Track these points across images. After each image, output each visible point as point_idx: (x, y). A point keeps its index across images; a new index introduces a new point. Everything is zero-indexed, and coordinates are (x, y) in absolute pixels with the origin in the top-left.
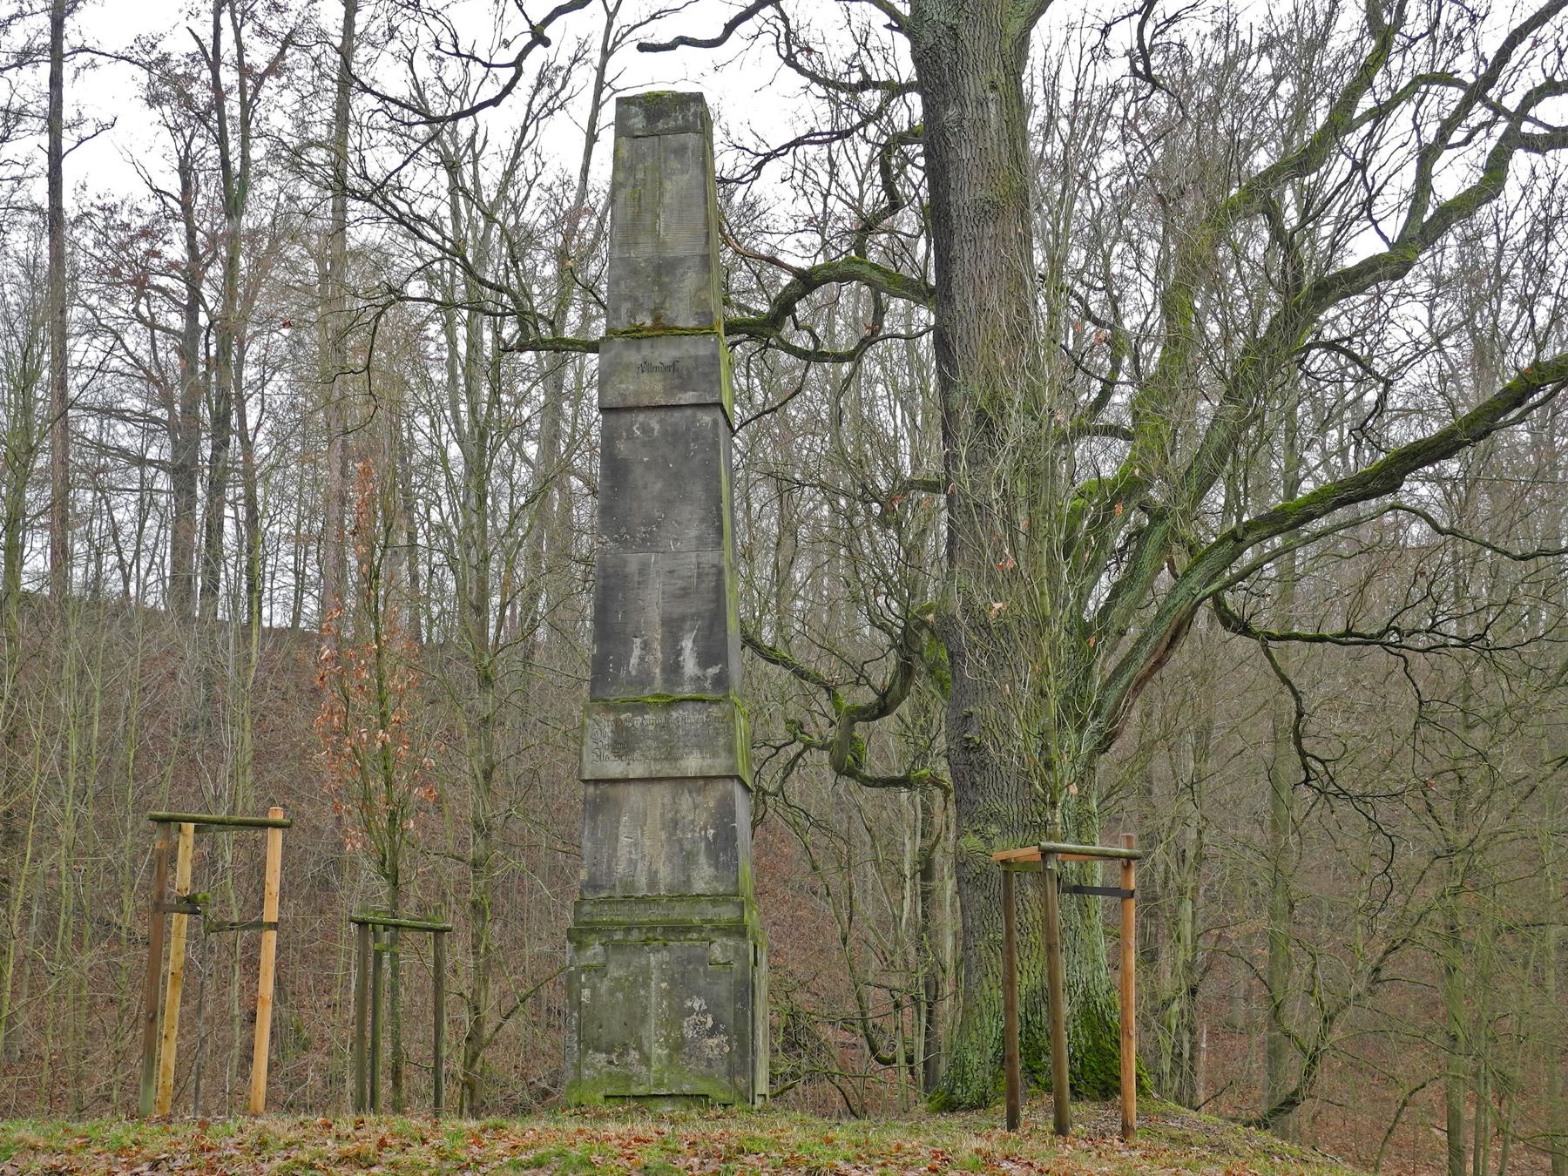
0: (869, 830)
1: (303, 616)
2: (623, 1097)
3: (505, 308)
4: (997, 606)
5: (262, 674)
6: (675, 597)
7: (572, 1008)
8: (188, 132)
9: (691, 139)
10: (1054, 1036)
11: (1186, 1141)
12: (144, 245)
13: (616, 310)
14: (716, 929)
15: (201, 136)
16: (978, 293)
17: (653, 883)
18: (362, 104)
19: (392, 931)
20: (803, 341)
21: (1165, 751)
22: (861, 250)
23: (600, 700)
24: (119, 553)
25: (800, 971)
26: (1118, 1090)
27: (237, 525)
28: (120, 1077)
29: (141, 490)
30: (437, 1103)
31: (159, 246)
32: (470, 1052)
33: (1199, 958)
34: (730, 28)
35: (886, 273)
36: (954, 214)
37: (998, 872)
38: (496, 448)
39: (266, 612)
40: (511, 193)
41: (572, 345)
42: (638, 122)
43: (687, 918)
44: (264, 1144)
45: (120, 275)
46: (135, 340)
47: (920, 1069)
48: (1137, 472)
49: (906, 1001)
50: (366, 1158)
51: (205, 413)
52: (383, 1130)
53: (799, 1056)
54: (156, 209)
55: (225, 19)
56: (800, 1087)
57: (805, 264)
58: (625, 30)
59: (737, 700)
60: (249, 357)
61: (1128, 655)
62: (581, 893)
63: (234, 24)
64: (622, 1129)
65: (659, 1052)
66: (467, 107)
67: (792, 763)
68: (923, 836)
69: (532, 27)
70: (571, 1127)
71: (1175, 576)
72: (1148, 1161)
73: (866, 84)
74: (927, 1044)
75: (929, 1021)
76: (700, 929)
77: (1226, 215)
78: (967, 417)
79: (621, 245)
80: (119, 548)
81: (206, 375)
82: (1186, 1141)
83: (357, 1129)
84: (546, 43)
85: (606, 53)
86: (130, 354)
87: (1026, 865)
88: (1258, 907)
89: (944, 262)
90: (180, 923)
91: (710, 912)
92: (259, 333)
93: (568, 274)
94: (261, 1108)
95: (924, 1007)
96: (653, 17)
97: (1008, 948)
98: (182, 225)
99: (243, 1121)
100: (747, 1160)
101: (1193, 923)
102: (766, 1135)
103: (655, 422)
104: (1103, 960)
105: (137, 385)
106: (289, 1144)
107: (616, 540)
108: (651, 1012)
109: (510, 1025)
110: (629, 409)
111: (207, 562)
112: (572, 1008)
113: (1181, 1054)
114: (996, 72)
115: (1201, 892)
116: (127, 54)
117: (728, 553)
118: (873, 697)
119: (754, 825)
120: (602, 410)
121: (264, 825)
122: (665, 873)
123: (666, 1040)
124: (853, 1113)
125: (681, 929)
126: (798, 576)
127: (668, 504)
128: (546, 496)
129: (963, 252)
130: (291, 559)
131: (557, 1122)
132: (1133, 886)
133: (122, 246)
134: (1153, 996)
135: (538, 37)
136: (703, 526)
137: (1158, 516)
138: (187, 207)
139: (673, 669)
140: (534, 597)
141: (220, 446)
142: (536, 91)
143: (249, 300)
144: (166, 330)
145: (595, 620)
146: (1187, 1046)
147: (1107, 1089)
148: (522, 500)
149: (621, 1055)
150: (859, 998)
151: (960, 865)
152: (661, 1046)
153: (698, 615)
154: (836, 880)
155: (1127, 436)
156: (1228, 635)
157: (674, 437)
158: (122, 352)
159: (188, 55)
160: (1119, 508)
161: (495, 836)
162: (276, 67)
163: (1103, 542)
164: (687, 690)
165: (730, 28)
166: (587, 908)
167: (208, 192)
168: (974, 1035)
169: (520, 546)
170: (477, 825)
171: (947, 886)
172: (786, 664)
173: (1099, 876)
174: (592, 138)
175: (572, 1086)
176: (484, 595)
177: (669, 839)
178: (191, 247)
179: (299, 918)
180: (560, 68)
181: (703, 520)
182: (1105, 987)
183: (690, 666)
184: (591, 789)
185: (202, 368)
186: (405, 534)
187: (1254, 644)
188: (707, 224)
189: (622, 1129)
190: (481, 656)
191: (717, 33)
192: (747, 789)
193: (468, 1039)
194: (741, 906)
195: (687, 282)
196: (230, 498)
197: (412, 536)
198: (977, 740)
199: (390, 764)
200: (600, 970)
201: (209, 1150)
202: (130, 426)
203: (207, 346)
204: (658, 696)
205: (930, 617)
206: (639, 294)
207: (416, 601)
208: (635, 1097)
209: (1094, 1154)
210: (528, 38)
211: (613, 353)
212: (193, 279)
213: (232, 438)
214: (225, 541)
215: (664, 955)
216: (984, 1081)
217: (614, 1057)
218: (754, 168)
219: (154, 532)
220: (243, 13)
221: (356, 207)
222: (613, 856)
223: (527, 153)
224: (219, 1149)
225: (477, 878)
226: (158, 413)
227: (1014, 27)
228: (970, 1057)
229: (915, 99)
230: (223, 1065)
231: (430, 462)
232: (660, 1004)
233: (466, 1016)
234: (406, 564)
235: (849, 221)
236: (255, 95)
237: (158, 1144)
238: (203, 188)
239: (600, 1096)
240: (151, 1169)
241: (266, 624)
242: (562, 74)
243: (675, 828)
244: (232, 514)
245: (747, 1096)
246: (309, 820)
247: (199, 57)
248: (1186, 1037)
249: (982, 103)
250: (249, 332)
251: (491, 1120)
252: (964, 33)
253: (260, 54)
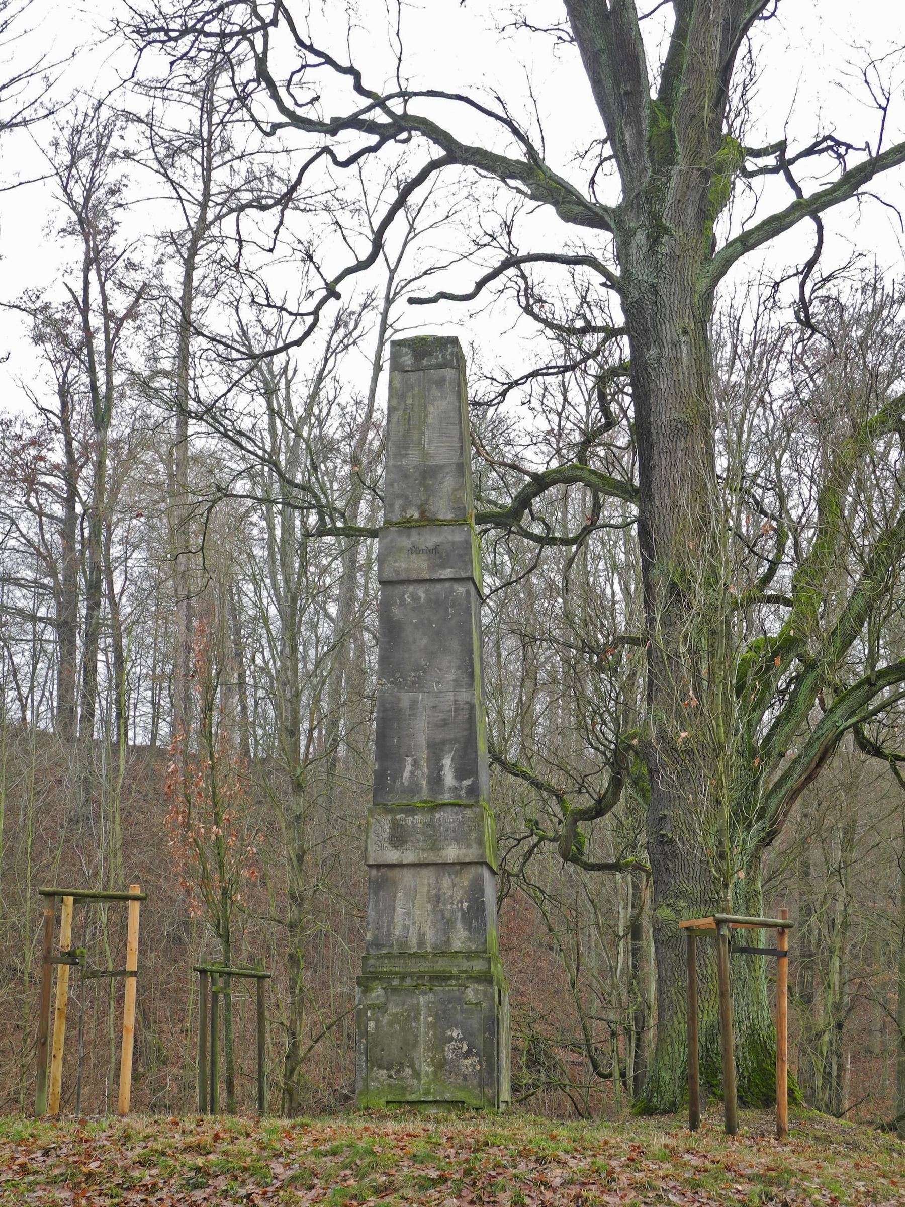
0: (592, 902)
1: (159, 737)
2: (400, 1102)
3: (310, 503)
4: (684, 734)
5: (128, 781)
6: (437, 726)
7: (361, 1036)
8: (65, 364)
9: (449, 373)
10: (726, 1059)
11: (827, 1140)
12: (33, 452)
13: (392, 506)
14: (469, 977)
15: (75, 367)
16: (672, 493)
17: (421, 943)
18: (197, 344)
19: (225, 977)
20: (537, 529)
21: (819, 844)
22: (582, 458)
23: (380, 804)
24: (18, 688)
25: (540, 1007)
26: (775, 1100)
27: (108, 667)
28: (25, 1084)
29: (33, 640)
30: (261, 1107)
31: (44, 453)
32: (289, 1067)
33: (846, 999)
34: (480, 285)
35: (601, 476)
36: (654, 432)
37: (685, 934)
38: (303, 610)
39: (130, 734)
40: (316, 411)
41: (361, 532)
42: (408, 360)
43: (448, 969)
44: (128, 1137)
45: (15, 475)
46: (27, 524)
47: (630, 1082)
48: (792, 633)
49: (620, 1031)
50: (205, 1147)
51: (81, 581)
52: (218, 1127)
53: (539, 1071)
54: (41, 423)
55: (93, 276)
56: (540, 1093)
57: (542, 469)
58: (403, 283)
59: (485, 804)
60: (115, 538)
61: (786, 772)
62: (367, 950)
63: (100, 279)
64: (397, 1127)
65: (426, 1069)
66: (280, 344)
67: (530, 852)
68: (633, 906)
69: (326, 284)
70: (360, 1125)
71: (824, 711)
72: (797, 1155)
73: (589, 328)
74: (636, 1063)
75: (638, 1046)
76: (457, 977)
77: (866, 433)
78: (661, 589)
79: (395, 455)
80: (17, 684)
81: (82, 552)
82: (827, 1140)
83: (198, 1126)
84: (338, 296)
85: (389, 301)
86: (23, 536)
87: (705, 932)
88: (889, 964)
89: (646, 470)
90: (63, 971)
91: (465, 964)
92: (123, 519)
93: (357, 478)
94: (127, 1110)
95: (634, 1036)
96: (425, 273)
97: (692, 992)
98: (61, 436)
99: (113, 1119)
100: (491, 1151)
101: (840, 973)
102: (506, 1132)
103: (421, 592)
104: (765, 1002)
105: (29, 560)
106: (147, 1137)
107: (392, 683)
108: (421, 1039)
109: (319, 1047)
110: (402, 582)
111: (84, 696)
112: (361, 1036)
113: (830, 1074)
114: (687, 321)
115: (847, 951)
116: (17, 303)
117: (478, 692)
118: (592, 803)
119: (500, 900)
120: (380, 583)
121: (126, 898)
122: (431, 936)
123: (432, 1061)
124: (580, 1114)
125: (443, 977)
126: (538, 707)
127: (432, 655)
128: (343, 646)
129: (661, 461)
130: (150, 693)
131: (349, 1121)
132: (786, 948)
133: (16, 452)
134: (809, 1029)
135: (332, 292)
136: (459, 672)
137: (811, 666)
138: (65, 422)
139: (436, 781)
140: (334, 723)
141: (94, 606)
142: (335, 330)
143: (114, 493)
144: (51, 517)
145: (377, 743)
146: (835, 1067)
147: (768, 1101)
148: (326, 648)
149: (398, 1071)
150: (584, 1028)
151: (657, 931)
152: (428, 1065)
153: (455, 740)
154: (567, 940)
155: (787, 603)
156: (863, 756)
157: (436, 603)
158: (17, 534)
159: (64, 304)
160: (778, 661)
161: (307, 905)
162: (132, 313)
163: (767, 685)
164: (447, 797)
165: (480, 285)
166: (372, 961)
167: (82, 410)
168: (666, 1058)
169: (324, 683)
170: (293, 897)
171: (650, 947)
172: (525, 776)
173: (763, 939)
174: (378, 368)
175: (361, 1094)
176: (296, 722)
177: (434, 909)
178: (69, 453)
179: (159, 966)
180: (353, 313)
181: (459, 668)
182: (766, 1023)
183: (449, 779)
184: (374, 872)
185: (78, 547)
186: (236, 675)
187: (887, 764)
188: (461, 439)
189: (397, 1127)
190: (295, 769)
191: (470, 289)
192: (493, 873)
193: (287, 1057)
194: (489, 960)
195: (446, 485)
196: (102, 646)
197: (242, 676)
198: (670, 835)
199: (222, 851)
200: (382, 1008)
201: (87, 1141)
202: (25, 591)
203: (82, 529)
204: (425, 801)
205: (635, 742)
206: (408, 493)
207: (245, 726)
208: (409, 1103)
209: (755, 1149)
210: (324, 293)
211: (389, 538)
212: (71, 477)
213: (103, 600)
214: (98, 679)
215: (431, 997)
216: (674, 1093)
217: (393, 1072)
218: (500, 394)
219: (44, 673)
220: (107, 270)
221: (193, 427)
222: (391, 921)
223: (328, 380)
224: (94, 1140)
225: (293, 936)
226: (46, 581)
227: (702, 285)
228: (663, 1074)
229: (625, 340)
230: (102, 1076)
231: (255, 618)
232: (427, 1033)
233: (285, 1039)
234: (237, 697)
235: (576, 437)
236: (116, 335)
237: (49, 1137)
238: (77, 407)
239: (382, 1102)
240: (43, 1155)
241: (131, 743)
242: (354, 317)
243: (438, 902)
244: (104, 658)
245: (494, 1103)
246: (165, 891)
247: (72, 305)
248: (834, 1060)
249: (676, 345)
250: (114, 519)
251: (299, 1120)
252: (663, 290)
253: (120, 303)
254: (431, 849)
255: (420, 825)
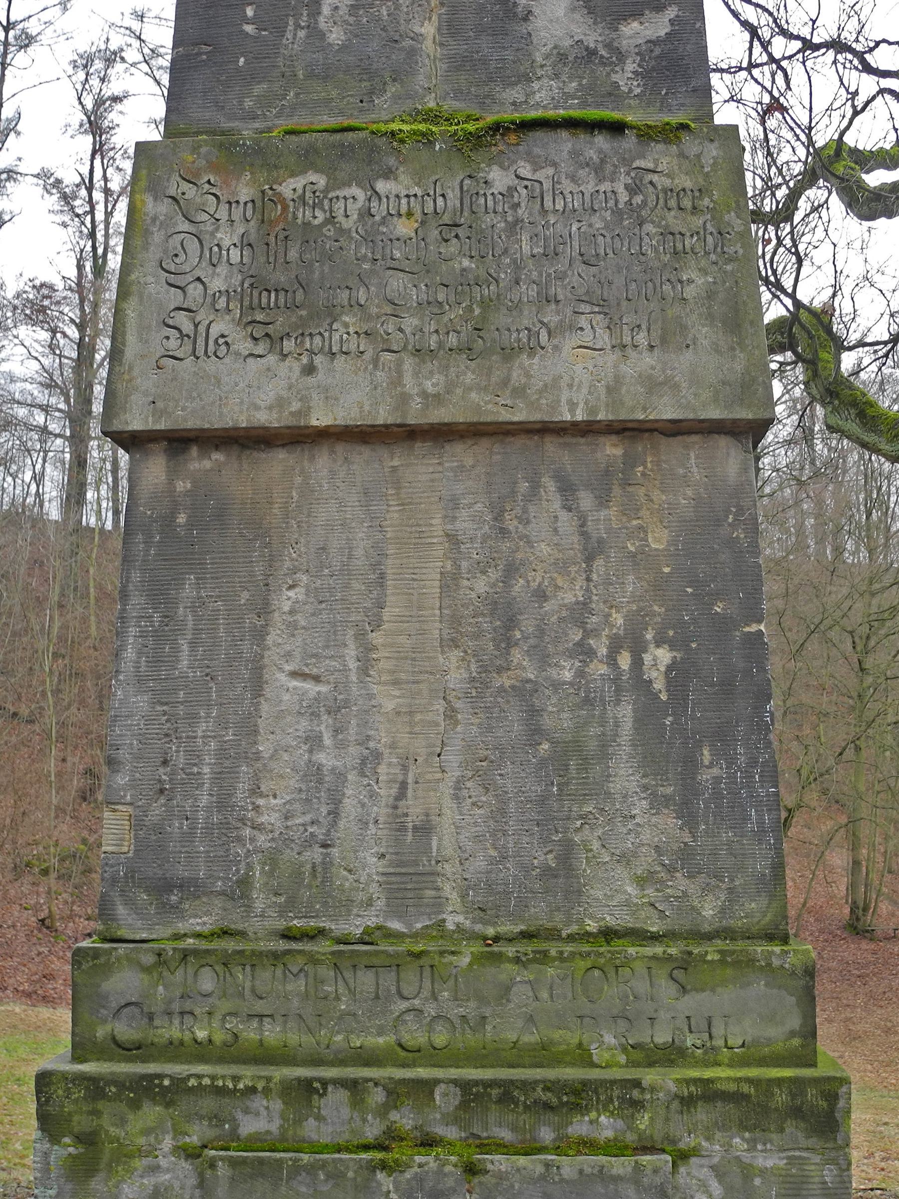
55: (97, 162)
243: (505, 642)
254: (467, 349)
255: (404, 228)
